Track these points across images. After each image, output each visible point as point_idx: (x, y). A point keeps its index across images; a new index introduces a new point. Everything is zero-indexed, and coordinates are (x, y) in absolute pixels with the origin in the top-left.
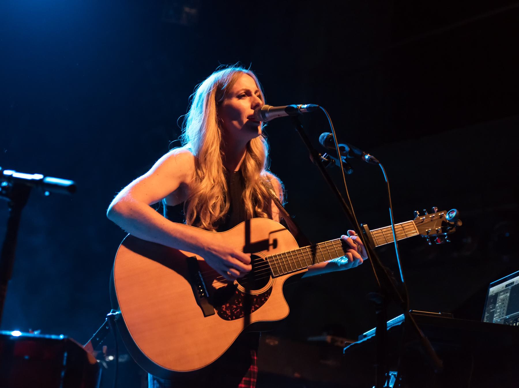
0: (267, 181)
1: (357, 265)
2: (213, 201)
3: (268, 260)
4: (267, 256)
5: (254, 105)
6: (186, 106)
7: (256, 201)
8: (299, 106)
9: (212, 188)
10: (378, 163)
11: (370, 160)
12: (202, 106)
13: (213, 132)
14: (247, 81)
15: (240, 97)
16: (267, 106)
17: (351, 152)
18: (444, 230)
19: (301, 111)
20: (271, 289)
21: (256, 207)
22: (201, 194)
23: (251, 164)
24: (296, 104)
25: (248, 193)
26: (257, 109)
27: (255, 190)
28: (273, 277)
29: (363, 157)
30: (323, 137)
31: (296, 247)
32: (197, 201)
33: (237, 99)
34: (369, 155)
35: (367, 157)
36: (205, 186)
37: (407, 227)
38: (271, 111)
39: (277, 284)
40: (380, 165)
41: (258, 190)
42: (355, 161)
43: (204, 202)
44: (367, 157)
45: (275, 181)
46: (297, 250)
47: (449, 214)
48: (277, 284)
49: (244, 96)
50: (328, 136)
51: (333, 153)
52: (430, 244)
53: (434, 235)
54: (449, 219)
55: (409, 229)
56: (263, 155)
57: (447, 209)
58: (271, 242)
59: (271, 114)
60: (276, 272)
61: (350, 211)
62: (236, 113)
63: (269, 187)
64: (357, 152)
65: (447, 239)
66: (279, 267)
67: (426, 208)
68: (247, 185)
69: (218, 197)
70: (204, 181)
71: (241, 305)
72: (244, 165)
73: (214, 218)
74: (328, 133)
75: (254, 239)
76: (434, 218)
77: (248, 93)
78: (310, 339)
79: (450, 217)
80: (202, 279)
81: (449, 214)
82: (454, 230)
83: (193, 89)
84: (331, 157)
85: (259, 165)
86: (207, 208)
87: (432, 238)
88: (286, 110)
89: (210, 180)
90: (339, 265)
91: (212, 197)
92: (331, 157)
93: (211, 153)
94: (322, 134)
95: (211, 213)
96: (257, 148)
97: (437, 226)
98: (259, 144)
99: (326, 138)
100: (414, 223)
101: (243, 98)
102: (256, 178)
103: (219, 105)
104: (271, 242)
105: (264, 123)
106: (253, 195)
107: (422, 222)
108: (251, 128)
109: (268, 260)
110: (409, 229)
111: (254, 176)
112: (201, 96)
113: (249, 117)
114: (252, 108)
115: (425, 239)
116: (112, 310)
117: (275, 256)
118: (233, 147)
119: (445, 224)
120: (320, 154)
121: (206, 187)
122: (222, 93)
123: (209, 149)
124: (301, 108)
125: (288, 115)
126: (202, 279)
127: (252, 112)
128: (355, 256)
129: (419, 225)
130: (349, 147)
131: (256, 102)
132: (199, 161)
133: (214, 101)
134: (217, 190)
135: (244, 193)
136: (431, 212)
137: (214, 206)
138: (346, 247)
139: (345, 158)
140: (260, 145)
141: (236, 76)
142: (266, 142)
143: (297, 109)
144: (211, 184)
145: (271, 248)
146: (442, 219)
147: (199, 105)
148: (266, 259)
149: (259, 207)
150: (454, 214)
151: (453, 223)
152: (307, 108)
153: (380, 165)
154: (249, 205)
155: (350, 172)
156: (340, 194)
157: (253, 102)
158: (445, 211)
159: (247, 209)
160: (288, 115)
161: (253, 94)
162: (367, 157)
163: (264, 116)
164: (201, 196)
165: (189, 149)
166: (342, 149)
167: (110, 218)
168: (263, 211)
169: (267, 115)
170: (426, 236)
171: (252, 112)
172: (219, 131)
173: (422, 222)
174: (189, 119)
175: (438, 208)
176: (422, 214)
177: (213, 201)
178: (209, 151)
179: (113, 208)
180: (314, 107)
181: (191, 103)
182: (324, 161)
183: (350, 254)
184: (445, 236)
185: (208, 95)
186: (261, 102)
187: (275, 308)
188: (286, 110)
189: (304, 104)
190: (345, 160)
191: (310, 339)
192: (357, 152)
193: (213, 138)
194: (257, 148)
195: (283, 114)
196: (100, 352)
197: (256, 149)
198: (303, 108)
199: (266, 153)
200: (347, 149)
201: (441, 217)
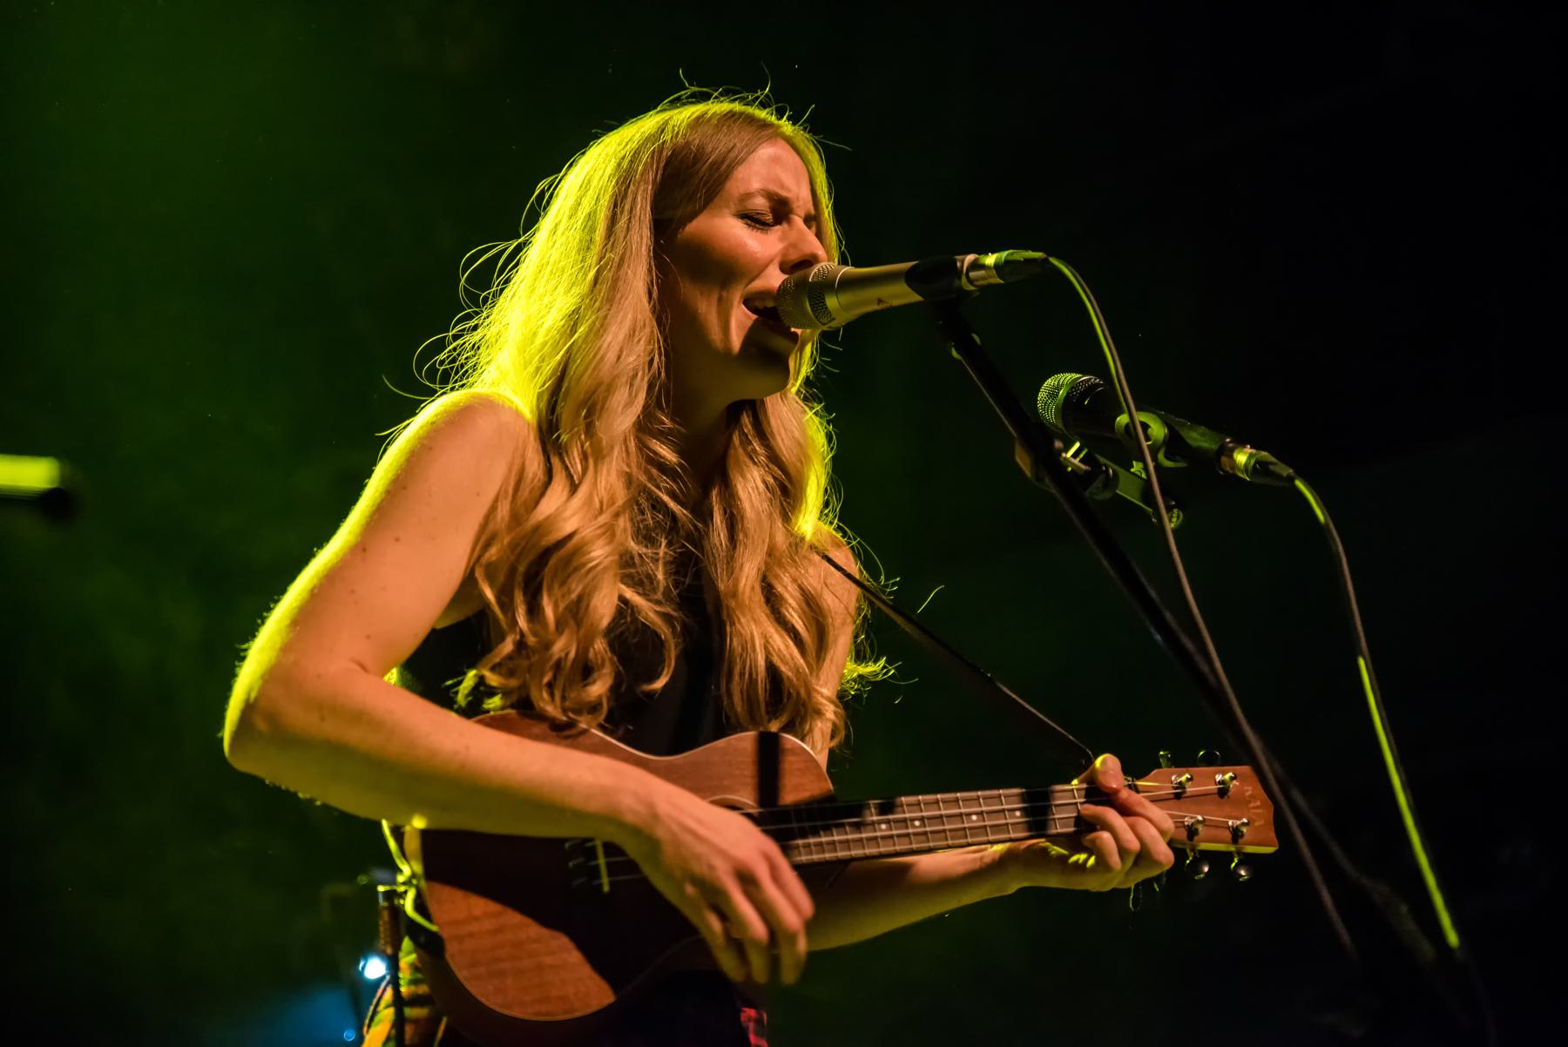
5: (794, 256)
10: (1291, 479)
11: (1259, 468)
13: (630, 344)
14: (782, 160)
17: (1174, 444)
19: (970, 281)
26: (799, 274)
29: (1224, 459)
30: (1053, 394)
38: (848, 284)
40: (1299, 484)
42: (1195, 479)
44: (1241, 457)
50: (1074, 386)
61: (1199, 659)
62: (721, 270)
64: (1199, 438)
78: (445, 1020)
88: (910, 278)
94: (1050, 382)
99: (1068, 397)
103: (665, 227)
108: (765, 353)
118: (701, 427)
130: (1166, 424)
141: (719, 144)
152: (997, 266)
153: (1299, 484)
156: (1153, 594)
167: (243, 765)
169: (832, 302)
179: (249, 708)
180: (1028, 261)
191: (445, 1020)
192: (1199, 438)
195: (901, 295)
196: (769, 218)
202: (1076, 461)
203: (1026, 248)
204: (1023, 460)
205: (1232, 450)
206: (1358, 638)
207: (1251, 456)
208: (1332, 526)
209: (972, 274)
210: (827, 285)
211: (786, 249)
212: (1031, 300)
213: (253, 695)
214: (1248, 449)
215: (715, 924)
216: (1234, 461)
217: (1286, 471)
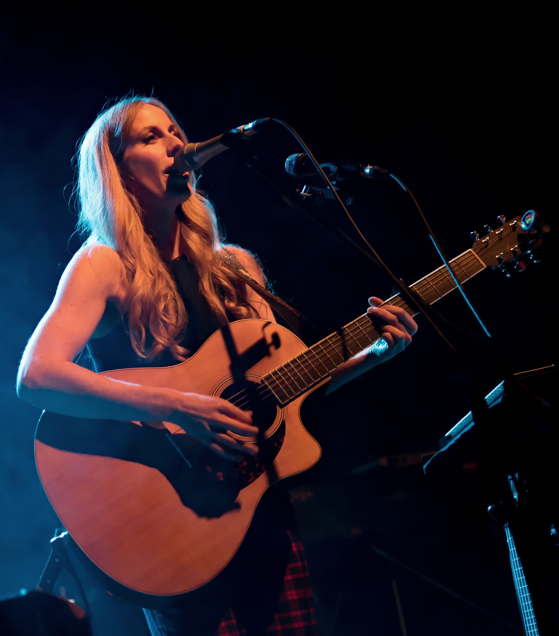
0: (228, 257)
1: (404, 348)
2: (162, 306)
3: (266, 383)
4: (263, 377)
5: (171, 148)
6: (72, 175)
7: (222, 292)
8: (241, 128)
9: (154, 283)
11: (373, 172)
12: (94, 169)
14: (152, 114)
15: (147, 141)
16: (191, 144)
17: (341, 172)
18: (523, 247)
20: (283, 425)
21: (226, 301)
22: (143, 296)
23: (194, 241)
24: (235, 128)
25: (206, 284)
26: (177, 154)
27: (214, 276)
28: (282, 407)
31: (303, 349)
32: (139, 309)
33: (143, 145)
34: (369, 167)
35: (367, 171)
36: (142, 283)
37: (465, 262)
38: (199, 150)
39: (291, 413)
40: (391, 175)
41: (220, 274)
42: (351, 182)
43: (149, 309)
45: (242, 255)
46: (306, 353)
47: (524, 220)
48: (291, 413)
49: (152, 138)
50: (297, 159)
51: (316, 181)
52: (508, 275)
53: (512, 260)
54: (526, 228)
55: (470, 260)
56: (208, 222)
57: (520, 213)
58: (269, 340)
59: (201, 155)
60: (283, 397)
62: (149, 165)
63: (233, 265)
65: (534, 258)
66: (286, 388)
67: (485, 220)
68: (200, 273)
69: (166, 296)
70: (137, 275)
71: (245, 464)
72: (184, 247)
73: (171, 328)
74: (296, 155)
75: (241, 348)
76: (503, 234)
77: (156, 133)
79: (527, 225)
80: (174, 444)
81: (524, 220)
82: (540, 242)
83: (74, 150)
84: (316, 189)
85: (207, 237)
86: (157, 315)
87: (509, 266)
88: (222, 141)
89: (145, 273)
90: (378, 354)
91: (158, 298)
92: (316, 189)
93: (131, 232)
95: (165, 322)
96: (196, 214)
97: (512, 245)
98: (198, 207)
100: (473, 252)
101: (151, 141)
102: (210, 257)
103: (119, 158)
104: (269, 340)
105: (197, 174)
106: (214, 284)
107: (486, 246)
108: (177, 188)
109: (266, 383)
110: (470, 260)
111: (204, 255)
112: (87, 152)
113: (169, 171)
114: (169, 156)
115: (499, 270)
116: (56, 531)
117: (275, 373)
119: (523, 238)
120: (297, 190)
121: (144, 283)
122: (118, 144)
123: (127, 225)
124: (244, 130)
125: (226, 148)
126: (174, 444)
127: (171, 160)
128: (396, 333)
129: (484, 250)
131: (174, 144)
132: (123, 245)
133: (111, 155)
134: (161, 286)
135: (200, 286)
136: (496, 225)
137: (166, 309)
138: (379, 325)
139: (334, 183)
140: (199, 208)
142: (207, 201)
143: (239, 133)
144: (150, 279)
145: (272, 349)
146: (517, 231)
147: (90, 168)
148: (262, 381)
149: (231, 300)
150: (531, 219)
151: (535, 232)
152: (253, 127)
153: (391, 175)
154: (214, 300)
155: (349, 202)
156: (349, 239)
157: (170, 145)
158: (518, 217)
159: (215, 309)
160: (226, 148)
161: (165, 131)
162: (367, 171)
163: (192, 162)
164: (142, 300)
165: (97, 242)
166: (327, 170)
168: (237, 305)
169: (196, 159)
170: (499, 266)
171: (171, 160)
172: (134, 199)
173: (486, 246)
174: (82, 193)
175: (505, 216)
176: (483, 234)
177: (162, 306)
178: (128, 230)
179: (24, 380)
180: (265, 122)
181: (78, 169)
182: (307, 197)
183: (388, 334)
184: (529, 255)
185: (99, 149)
186: (180, 142)
187: (300, 451)
188: (222, 141)
189: (247, 123)
190: (335, 185)
193: (127, 211)
194: (196, 214)
195: (220, 148)
197: (195, 216)
198: (248, 129)
199: (214, 219)
200: (333, 168)
201: (514, 228)
202: (306, 194)
203: (262, 117)
204: (286, 200)
205: (363, 169)
206: (475, 311)
207: (371, 169)
208: (410, 192)
209: (245, 133)
210: (191, 153)
211: (167, 148)
212: (269, 143)
213: (25, 374)
214: (369, 167)
215: (215, 446)
216: (365, 172)
217: (385, 171)
